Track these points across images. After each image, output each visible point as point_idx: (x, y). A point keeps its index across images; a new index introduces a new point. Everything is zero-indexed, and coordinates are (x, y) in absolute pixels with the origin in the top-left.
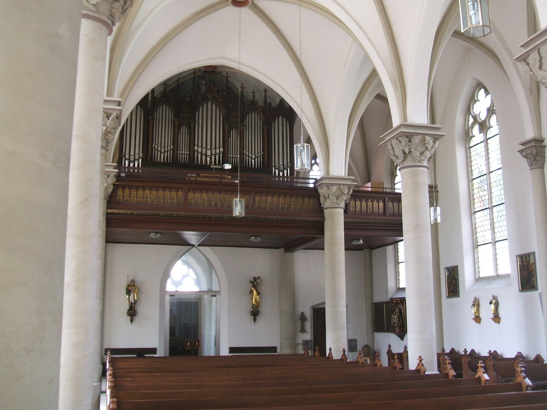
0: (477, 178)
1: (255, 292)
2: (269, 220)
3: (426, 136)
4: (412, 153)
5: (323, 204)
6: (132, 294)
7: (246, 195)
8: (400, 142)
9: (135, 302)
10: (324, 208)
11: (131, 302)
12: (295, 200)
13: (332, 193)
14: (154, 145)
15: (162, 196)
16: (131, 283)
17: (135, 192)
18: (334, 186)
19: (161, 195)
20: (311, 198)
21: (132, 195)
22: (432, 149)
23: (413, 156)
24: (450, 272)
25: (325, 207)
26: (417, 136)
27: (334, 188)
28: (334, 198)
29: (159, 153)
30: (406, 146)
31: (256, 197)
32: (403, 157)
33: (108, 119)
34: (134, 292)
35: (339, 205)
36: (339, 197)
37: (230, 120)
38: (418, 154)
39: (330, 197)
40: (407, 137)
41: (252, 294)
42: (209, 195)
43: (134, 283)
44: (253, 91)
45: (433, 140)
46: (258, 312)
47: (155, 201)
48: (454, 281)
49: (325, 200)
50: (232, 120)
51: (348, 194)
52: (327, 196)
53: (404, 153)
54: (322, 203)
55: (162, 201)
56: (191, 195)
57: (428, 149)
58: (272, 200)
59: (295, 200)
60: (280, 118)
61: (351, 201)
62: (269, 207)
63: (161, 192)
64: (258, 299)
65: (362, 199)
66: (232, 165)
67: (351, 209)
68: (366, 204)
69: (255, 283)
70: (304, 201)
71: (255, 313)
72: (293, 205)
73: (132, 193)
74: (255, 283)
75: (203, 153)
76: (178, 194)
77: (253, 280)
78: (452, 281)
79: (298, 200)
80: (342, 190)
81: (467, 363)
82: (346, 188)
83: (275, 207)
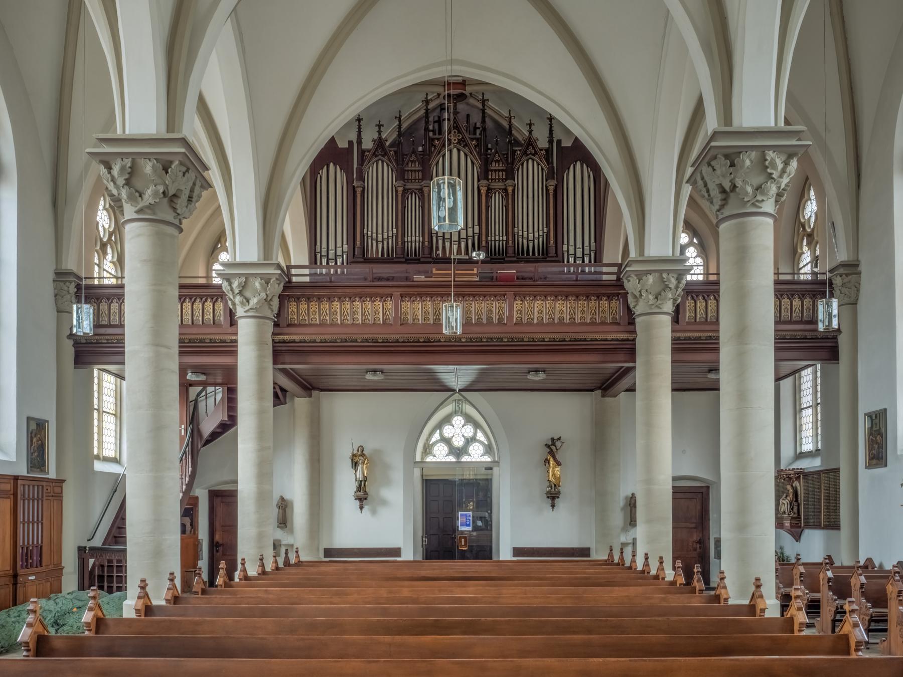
0: (359, 132)
1: (552, 462)
3: (766, 151)
4: (737, 189)
5: (634, 308)
6: (359, 468)
7: (498, 300)
8: (714, 170)
9: (365, 479)
10: (637, 315)
11: (358, 479)
12: (584, 304)
15: (359, 310)
16: (358, 451)
17: (317, 307)
18: (650, 274)
19: (379, 308)
20: (612, 300)
21: (311, 310)
22: (781, 176)
23: (739, 194)
24: (874, 421)
25: (637, 313)
26: (746, 152)
27: (651, 279)
28: (650, 297)
29: (374, 243)
30: (724, 176)
31: (516, 302)
32: (720, 198)
33: (167, 172)
34: (363, 463)
35: (661, 308)
36: (661, 295)
37: (490, 177)
38: (749, 189)
40: (727, 156)
41: (547, 464)
42: (436, 304)
43: (362, 451)
45: (784, 158)
46: (559, 492)
47: (349, 318)
48: (878, 438)
49: (637, 301)
50: (493, 177)
51: (677, 287)
52: (638, 294)
53: (723, 191)
54: (631, 306)
55: (359, 317)
56: (407, 306)
57: (773, 178)
58: (542, 307)
60: (578, 164)
61: (687, 302)
62: (538, 319)
63: (358, 303)
64: (558, 473)
65: (708, 296)
66: (487, 253)
67: (688, 314)
68: (716, 304)
69: (552, 447)
71: (553, 496)
72: (579, 313)
74: (553, 448)
77: (550, 443)
78: (876, 438)
80: (666, 282)
81: (858, 586)
82: (673, 277)
83: (549, 319)
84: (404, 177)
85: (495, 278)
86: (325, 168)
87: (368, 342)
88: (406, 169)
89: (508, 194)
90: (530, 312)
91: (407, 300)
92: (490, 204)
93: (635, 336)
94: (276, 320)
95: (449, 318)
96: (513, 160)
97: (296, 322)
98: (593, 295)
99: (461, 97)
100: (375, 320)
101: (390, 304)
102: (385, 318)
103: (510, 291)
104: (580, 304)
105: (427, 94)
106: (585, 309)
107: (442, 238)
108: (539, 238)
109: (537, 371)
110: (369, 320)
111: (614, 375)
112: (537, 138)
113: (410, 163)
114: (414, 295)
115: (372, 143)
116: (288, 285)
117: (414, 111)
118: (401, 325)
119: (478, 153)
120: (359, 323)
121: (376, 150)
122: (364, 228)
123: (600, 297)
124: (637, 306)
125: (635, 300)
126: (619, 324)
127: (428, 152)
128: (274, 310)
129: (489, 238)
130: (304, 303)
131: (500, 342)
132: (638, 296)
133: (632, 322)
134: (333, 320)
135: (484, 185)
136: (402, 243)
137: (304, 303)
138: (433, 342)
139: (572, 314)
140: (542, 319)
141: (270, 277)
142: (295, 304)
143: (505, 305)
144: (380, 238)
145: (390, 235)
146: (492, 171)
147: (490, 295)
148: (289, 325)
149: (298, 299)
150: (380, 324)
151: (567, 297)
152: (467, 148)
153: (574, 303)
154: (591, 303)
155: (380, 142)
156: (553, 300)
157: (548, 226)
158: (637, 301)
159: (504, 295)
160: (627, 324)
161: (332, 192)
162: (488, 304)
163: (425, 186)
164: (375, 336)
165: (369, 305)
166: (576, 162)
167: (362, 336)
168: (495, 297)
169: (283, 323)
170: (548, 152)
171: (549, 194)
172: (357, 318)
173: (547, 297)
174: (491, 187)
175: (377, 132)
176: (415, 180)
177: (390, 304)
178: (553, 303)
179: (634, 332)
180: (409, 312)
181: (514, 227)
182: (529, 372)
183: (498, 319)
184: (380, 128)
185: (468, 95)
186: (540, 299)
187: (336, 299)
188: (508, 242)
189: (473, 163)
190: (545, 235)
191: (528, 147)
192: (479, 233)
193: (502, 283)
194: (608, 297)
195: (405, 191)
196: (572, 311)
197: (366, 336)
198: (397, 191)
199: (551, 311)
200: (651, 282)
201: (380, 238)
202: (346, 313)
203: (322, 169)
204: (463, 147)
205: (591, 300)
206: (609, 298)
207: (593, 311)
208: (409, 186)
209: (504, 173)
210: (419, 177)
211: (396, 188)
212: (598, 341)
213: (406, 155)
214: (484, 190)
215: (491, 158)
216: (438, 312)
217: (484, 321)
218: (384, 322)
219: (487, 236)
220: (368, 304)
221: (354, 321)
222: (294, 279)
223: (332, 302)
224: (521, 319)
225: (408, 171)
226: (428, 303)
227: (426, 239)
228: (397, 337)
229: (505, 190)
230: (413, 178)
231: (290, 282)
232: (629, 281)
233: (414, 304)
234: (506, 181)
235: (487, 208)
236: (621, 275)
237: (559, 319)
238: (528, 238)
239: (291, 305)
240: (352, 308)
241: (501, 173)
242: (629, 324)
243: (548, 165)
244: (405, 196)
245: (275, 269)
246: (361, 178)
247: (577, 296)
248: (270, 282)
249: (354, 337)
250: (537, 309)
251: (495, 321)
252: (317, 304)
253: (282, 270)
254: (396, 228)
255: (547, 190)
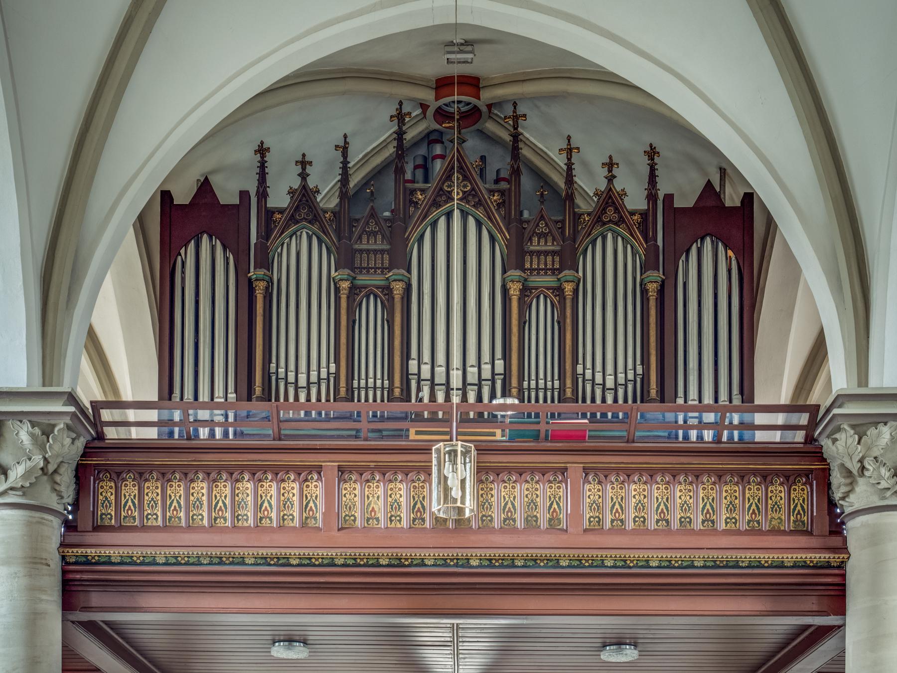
2: (634, 567)
12: (735, 491)
13: (875, 455)
14: (273, 365)
15: (249, 498)
17: (159, 491)
18: (886, 424)
19: (294, 495)
20: (794, 483)
21: (146, 498)
25: (848, 510)
31: (587, 487)
39: (868, 470)
42: (415, 487)
44: (608, 161)
47: (228, 515)
49: (852, 484)
52: (854, 467)
54: (837, 495)
55: (249, 514)
58: (645, 497)
59: (735, 491)
62: (635, 521)
63: (247, 485)
70: (770, 495)
72: (724, 511)
73: (147, 495)
75: (437, 381)
76: (305, 489)
79: (747, 491)
84: (353, 262)
85: (542, 435)
86: (192, 246)
87: (270, 565)
88: (356, 247)
89: (565, 299)
90: (617, 506)
91: (354, 478)
92: (527, 318)
93: (846, 556)
94: (70, 517)
95: (446, 478)
96: (575, 232)
97: (113, 521)
98: (755, 472)
99: (472, 115)
100: (284, 520)
101: (316, 487)
102: (304, 515)
103: (575, 464)
104: (726, 491)
105: (401, 104)
106: (737, 501)
107: (429, 382)
108: (626, 386)
109: (619, 643)
110: (271, 519)
111: (773, 656)
112: (623, 190)
113: (365, 237)
114: (368, 468)
115: (289, 197)
116: (97, 444)
117: (374, 148)
118: (339, 530)
119: (504, 219)
120: (250, 526)
121: (295, 210)
122: (270, 362)
123: (769, 478)
124: (852, 496)
125: (848, 481)
126: (809, 533)
127: (401, 216)
128: (65, 494)
129: (526, 384)
130: (130, 483)
131: (553, 567)
132: (855, 472)
133: (836, 529)
134: (193, 520)
135: (517, 278)
136: (347, 390)
137: (130, 483)
138: (409, 566)
139: (708, 511)
140: (644, 522)
141: (52, 422)
142: (113, 484)
143: (563, 492)
144: (302, 382)
145: (324, 375)
146: (532, 253)
147: (533, 471)
148: (97, 528)
149: (119, 474)
150: (295, 528)
151: (697, 477)
152: (481, 209)
153: (712, 489)
154: (750, 489)
155: (304, 195)
156: (668, 483)
157: (645, 362)
158: (851, 484)
159: (564, 470)
160: (827, 533)
161: (219, 314)
162: (527, 489)
163: (395, 280)
164: (283, 551)
165: (271, 489)
166: (703, 239)
167: (256, 551)
168: (543, 475)
169: (85, 523)
170: (646, 219)
171: (648, 299)
172: (246, 515)
173: (654, 476)
174: (531, 284)
175: (299, 175)
176: (376, 268)
177: (316, 487)
178: (667, 489)
179: (844, 549)
180: (358, 504)
181: (575, 362)
182: (604, 646)
183: (550, 520)
184: (304, 169)
185: (484, 109)
186: (639, 480)
187: (201, 476)
188: (564, 391)
189: (493, 239)
190: (638, 380)
191: (604, 209)
192: (505, 374)
193: (559, 445)
194: (787, 478)
195: (354, 290)
196: (708, 506)
197: (264, 552)
198: (337, 290)
199: (662, 506)
200: (886, 440)
201: (302, 382)
202: (220, 504)
203: (186, 246)
204: (474, 206)
205: (749, 483)
206: (788, 481)
207: (754, 507)
208: (363, 279)
209: (557, 259)
210: (382, 264)
211: (335, 284)
212: (763, 567)
213: (357, 221)
214: (515, 290)
215: (528, 230)
216: (419, 505)
217: (520, 524)
218: (304, 525)
219: (521, 379)
220: (270, 486)
221: (238, 520)
222: (111, 433)
223: (192, 481)
224: (599, 522)
225: (361, 251)
226: (399, 485)
227: (397, 383)
228: (332, 553)
229: (559, 290)
230: (372, 265)
231: (100, 436)
232: (835, 441)
233: (369, 487)
234: (560, 273)
235: (522, 323)
236: (814, 430)
237: (681, 522)
238: (604, 384)
239: (102, 487)
240: (234, 495)
241: (549, 259)
242: (832, 533)
243: (646, 243)
244: (354, 300)
245: (65, 405)
246: (265, 262)
247: (720, 475)
248: (52, 432)
249: (237, 552)
250: (634, 500)
251: (543, 524)
252: (159, 485)
253: (83, 411)
254: (335, 362)
255: (644, 292)
